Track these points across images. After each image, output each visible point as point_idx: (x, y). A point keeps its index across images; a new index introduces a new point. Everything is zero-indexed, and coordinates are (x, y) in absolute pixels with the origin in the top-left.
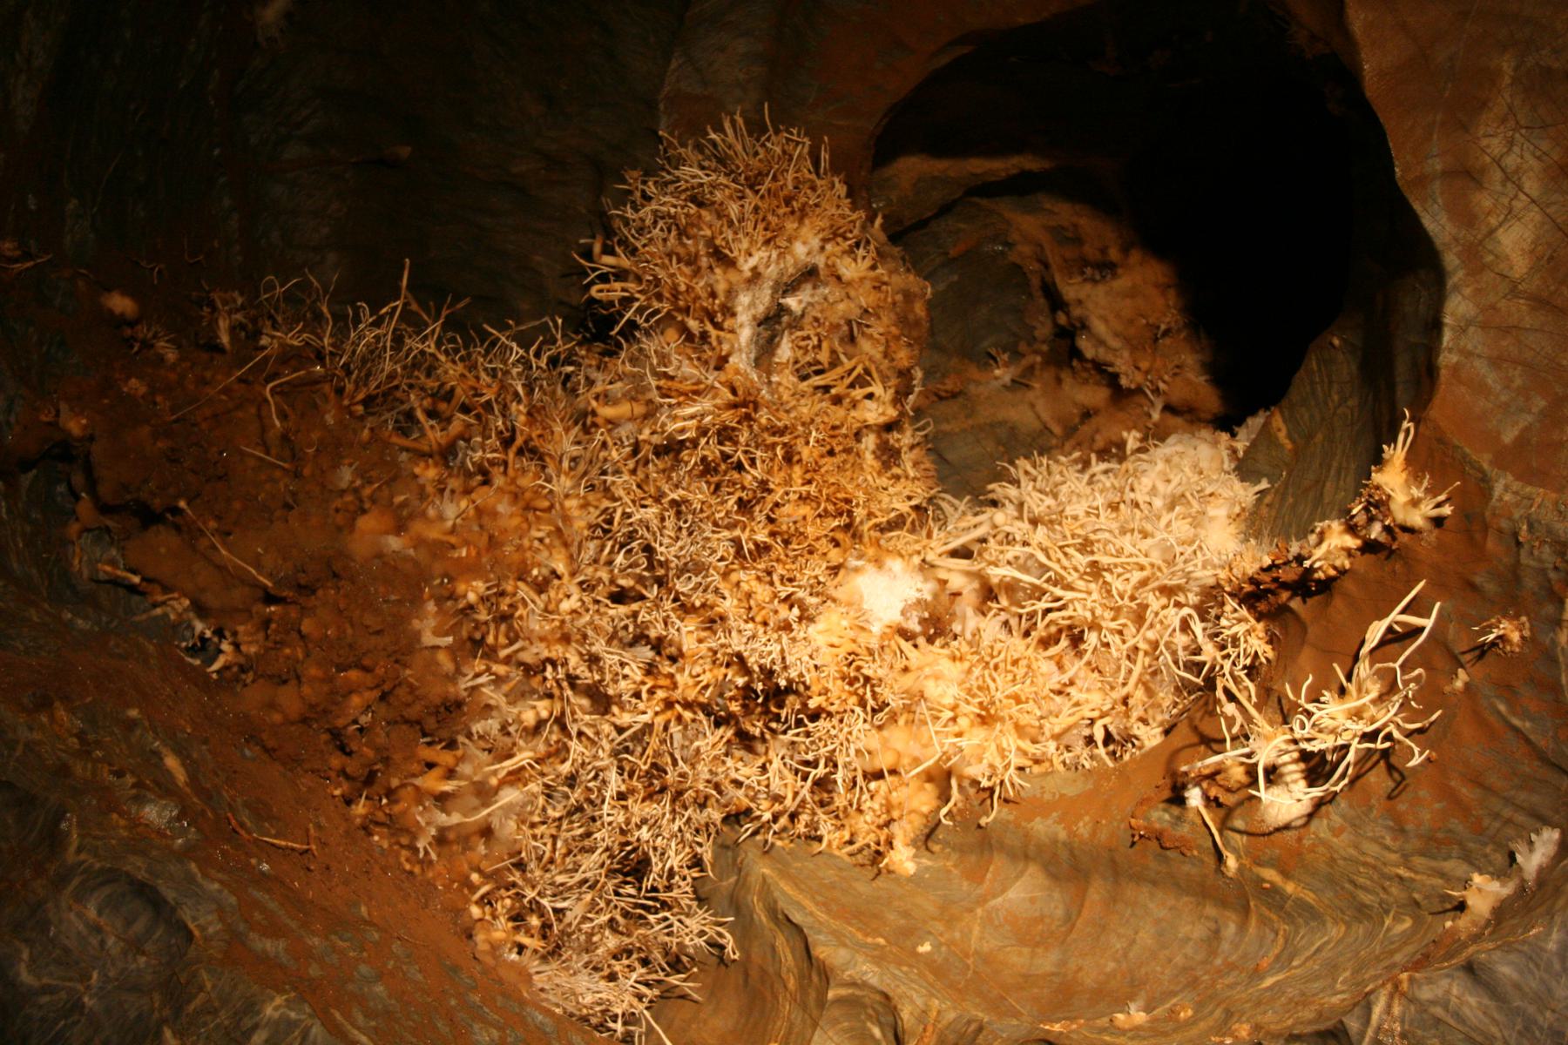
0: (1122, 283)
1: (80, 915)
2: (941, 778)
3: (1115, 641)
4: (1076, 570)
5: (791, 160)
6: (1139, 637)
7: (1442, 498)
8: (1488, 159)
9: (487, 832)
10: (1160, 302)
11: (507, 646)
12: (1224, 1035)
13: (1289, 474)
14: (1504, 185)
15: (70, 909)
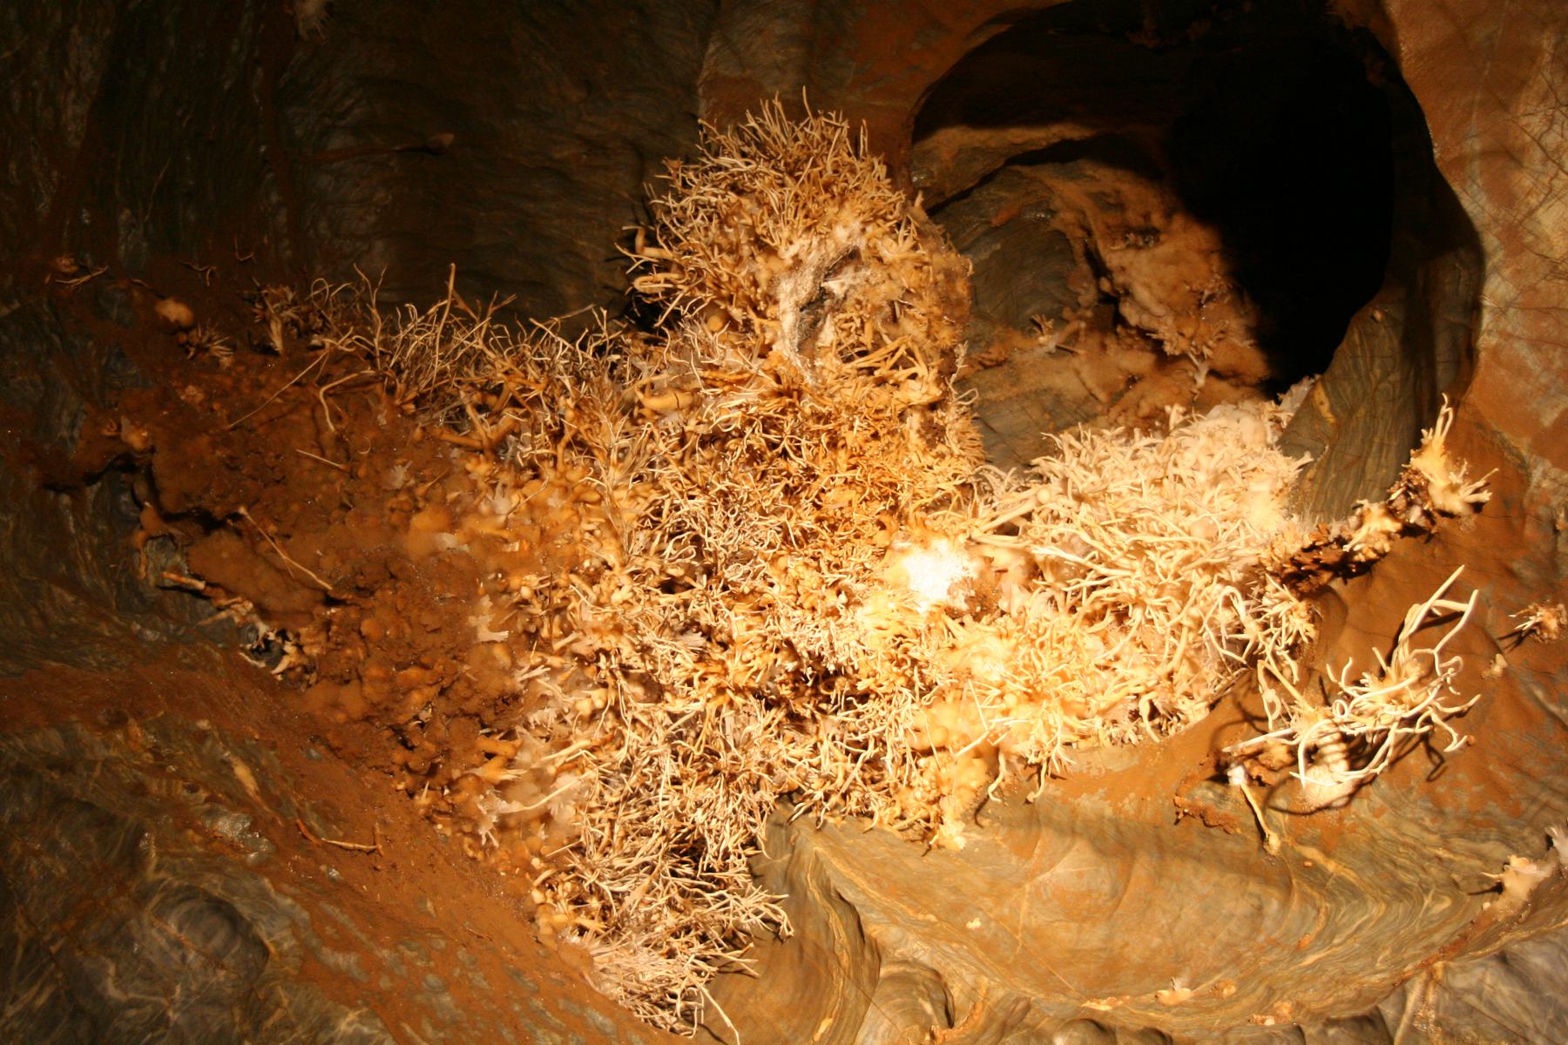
0: (1165, 249)
1: (161, 931)
2: (990, 755)
3: (1157, 618)
4: (1120, 549)
5: (830, 143)
6: (1183, 614)
7: (1480, 484)
8: (1528, 139)
9: (546, 818)
10: (1203, 267)
11: (560, 638)
12: (1266, 1013)
13: (1332, 448)
14: (1544, 165)
15: (152, 926)
